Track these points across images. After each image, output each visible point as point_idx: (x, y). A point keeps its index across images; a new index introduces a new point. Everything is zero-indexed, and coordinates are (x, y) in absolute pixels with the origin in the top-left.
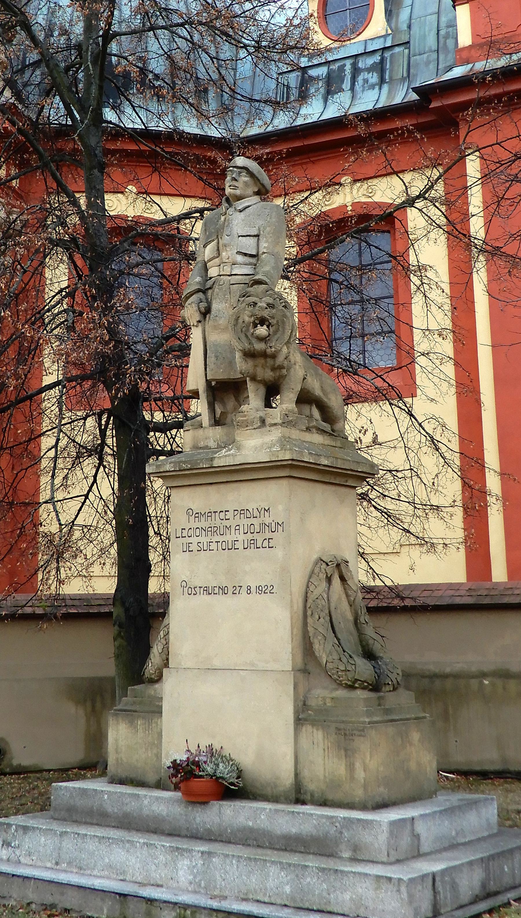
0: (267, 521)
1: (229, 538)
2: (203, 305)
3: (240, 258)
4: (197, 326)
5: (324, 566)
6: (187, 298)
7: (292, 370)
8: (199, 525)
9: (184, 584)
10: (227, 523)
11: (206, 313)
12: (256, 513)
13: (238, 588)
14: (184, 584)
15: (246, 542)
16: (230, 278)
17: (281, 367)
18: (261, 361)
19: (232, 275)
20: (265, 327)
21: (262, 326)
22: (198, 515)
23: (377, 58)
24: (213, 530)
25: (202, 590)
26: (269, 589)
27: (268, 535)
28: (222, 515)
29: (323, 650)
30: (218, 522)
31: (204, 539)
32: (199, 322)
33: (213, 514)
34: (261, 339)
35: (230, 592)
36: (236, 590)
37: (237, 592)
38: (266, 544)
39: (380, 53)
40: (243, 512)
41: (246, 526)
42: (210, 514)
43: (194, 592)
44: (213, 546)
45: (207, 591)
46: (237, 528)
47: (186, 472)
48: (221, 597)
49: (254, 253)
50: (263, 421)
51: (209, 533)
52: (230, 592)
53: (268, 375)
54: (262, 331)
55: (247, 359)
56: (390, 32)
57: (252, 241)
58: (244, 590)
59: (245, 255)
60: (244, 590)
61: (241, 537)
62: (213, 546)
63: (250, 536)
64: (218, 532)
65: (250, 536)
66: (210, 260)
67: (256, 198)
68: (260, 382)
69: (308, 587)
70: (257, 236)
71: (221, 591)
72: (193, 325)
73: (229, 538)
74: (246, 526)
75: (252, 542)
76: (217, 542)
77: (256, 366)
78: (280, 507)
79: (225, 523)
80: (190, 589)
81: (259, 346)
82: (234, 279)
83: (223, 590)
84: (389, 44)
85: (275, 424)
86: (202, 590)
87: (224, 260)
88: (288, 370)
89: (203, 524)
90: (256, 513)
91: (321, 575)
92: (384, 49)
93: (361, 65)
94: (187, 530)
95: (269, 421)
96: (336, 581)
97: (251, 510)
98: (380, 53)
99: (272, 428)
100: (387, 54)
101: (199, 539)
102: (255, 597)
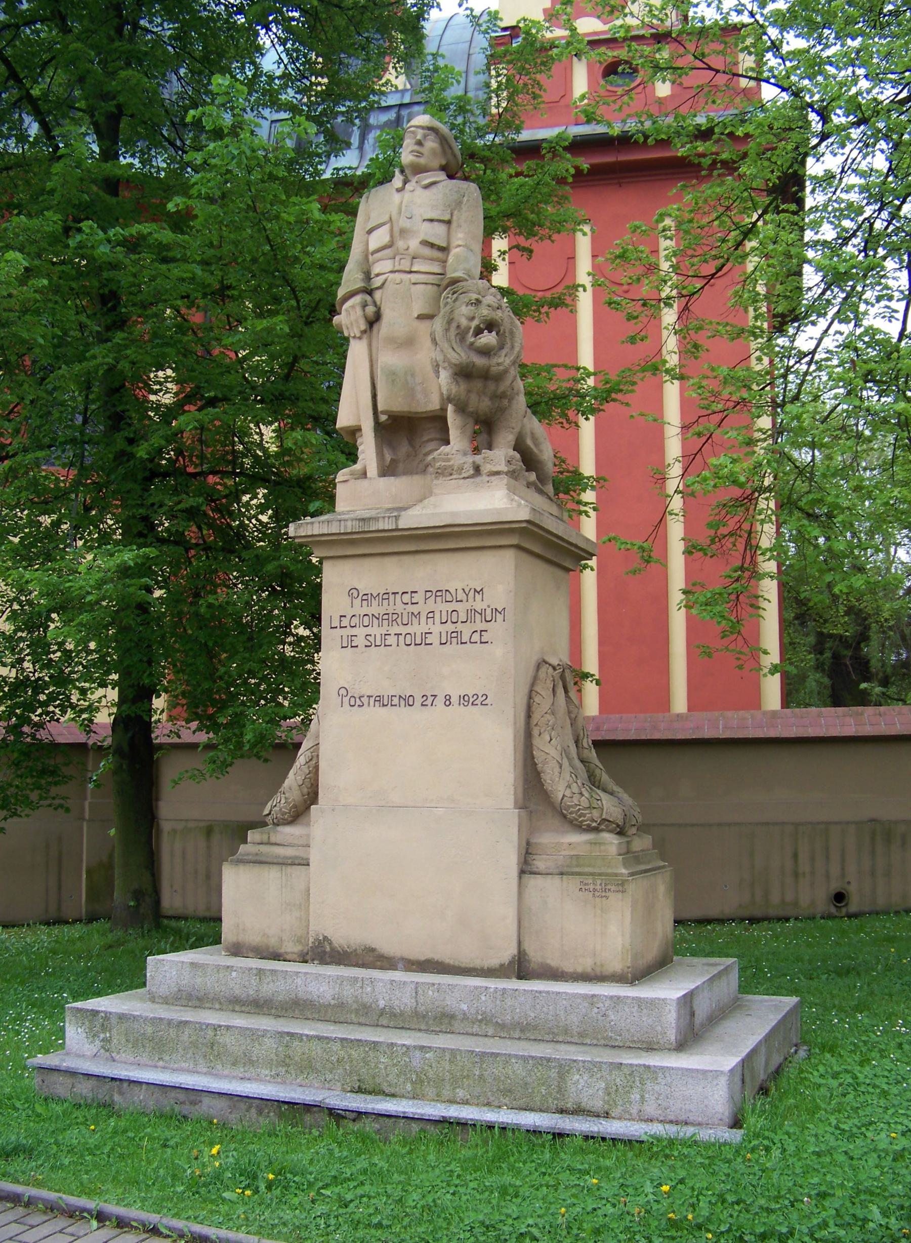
0: (479, 606)
1: (417, 628)
2: (371, 309)
3: (427, 251)
4: (360, 338)
5: (551, 670)
6: (346, 298)
7: (514, 402)
8: (365, 610)
9: (343, 692)
10: (415, 609)
11: (373, 321)
12: (461, 595)
13: (430, 699)
14: (343, 692)
15: (444, 635)
16: (409, 276)
17: (503, 396)
18: (478, 384)
19: (411, 272)
20: (494, 333)
21: (490, 332)
22: (367, 598)
23: (392, 115)
24: (391, 618)
25: (372, 700)
26: (481, 699)
27: (480, 626)
28: (406, 598)
29: (562, 782)
30: (400, 608)
31: (376, 631)
32: (364, 332)
33: (392, 597)
34: (486, 352)
35: (418, 703)
36: (428, 700)
37: (429, 702)
38: (476, 637)
39: (396, 110)
40: (440, 594)
41: (444, 613)
42: (386, 596)
43: (358, 702)
44: (391, 640)
45: (380, 701)
46: (431, 615)
47: (355, 536)
48: (404, 711)
49: (444, 245)
50: (477, 469)
51: (385, 622)
52: (418, 703)
53: (484, 405)
54: (488, 339)
55: (459, 379)
56: (408, 86)
57: (441, 229)
58: (440, 700)
59: (432, 245)
60: (440, 700)
61: (437, 628)
62: (391, 640)
63: (450, 627)
64: (399, 620)
65: (450, 627)
66: (373, 253)
67: (442, 176)
68: (470, 414)
69: (530, 697)
70: (449, 222)
71: (402, 702)
72: (354, 337)
73: (417, 628)
74: (444, 613)
75: (454, 635)
76: (398, 635)
77: (469, 391)
78: (500, 588)
79: (411, 608)
80: (353, 700)
81: (480, 361)
82: (414, 278)
83: (407, 701)
84: (407, 100)
85: (497, 473)
86: (372, 700)
87: (402, 251)
88: (510, 401)
89: (375, 609)
90: (461, 595)
91: (548, 682)
92: (401, 106)
93: (372, 121)
94: (349, 617)
95: (486, 468)
96: (560, 691)
97: (453, 591)
98: (396, 110)
99: (493, 478)
100: (404, 112)
101: (369, 630)
102: (456, 709)
